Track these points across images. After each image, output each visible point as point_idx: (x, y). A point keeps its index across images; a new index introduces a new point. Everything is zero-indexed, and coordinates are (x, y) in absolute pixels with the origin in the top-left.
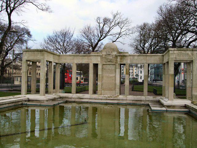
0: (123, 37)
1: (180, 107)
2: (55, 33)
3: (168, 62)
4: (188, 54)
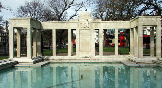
0: (85, 7)
1: (148, 63)
2: (27, 4)
3: (137, 28)
4: (153, 20)
